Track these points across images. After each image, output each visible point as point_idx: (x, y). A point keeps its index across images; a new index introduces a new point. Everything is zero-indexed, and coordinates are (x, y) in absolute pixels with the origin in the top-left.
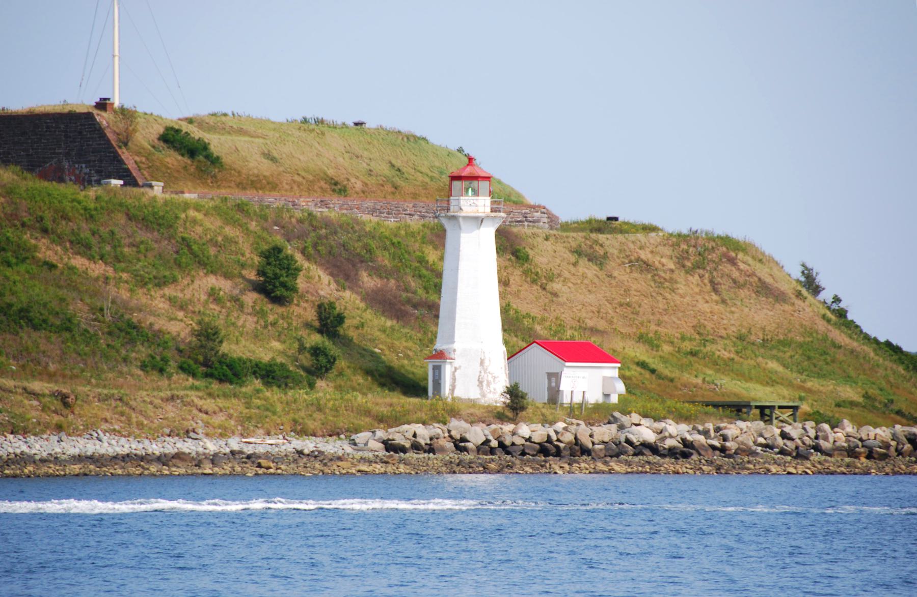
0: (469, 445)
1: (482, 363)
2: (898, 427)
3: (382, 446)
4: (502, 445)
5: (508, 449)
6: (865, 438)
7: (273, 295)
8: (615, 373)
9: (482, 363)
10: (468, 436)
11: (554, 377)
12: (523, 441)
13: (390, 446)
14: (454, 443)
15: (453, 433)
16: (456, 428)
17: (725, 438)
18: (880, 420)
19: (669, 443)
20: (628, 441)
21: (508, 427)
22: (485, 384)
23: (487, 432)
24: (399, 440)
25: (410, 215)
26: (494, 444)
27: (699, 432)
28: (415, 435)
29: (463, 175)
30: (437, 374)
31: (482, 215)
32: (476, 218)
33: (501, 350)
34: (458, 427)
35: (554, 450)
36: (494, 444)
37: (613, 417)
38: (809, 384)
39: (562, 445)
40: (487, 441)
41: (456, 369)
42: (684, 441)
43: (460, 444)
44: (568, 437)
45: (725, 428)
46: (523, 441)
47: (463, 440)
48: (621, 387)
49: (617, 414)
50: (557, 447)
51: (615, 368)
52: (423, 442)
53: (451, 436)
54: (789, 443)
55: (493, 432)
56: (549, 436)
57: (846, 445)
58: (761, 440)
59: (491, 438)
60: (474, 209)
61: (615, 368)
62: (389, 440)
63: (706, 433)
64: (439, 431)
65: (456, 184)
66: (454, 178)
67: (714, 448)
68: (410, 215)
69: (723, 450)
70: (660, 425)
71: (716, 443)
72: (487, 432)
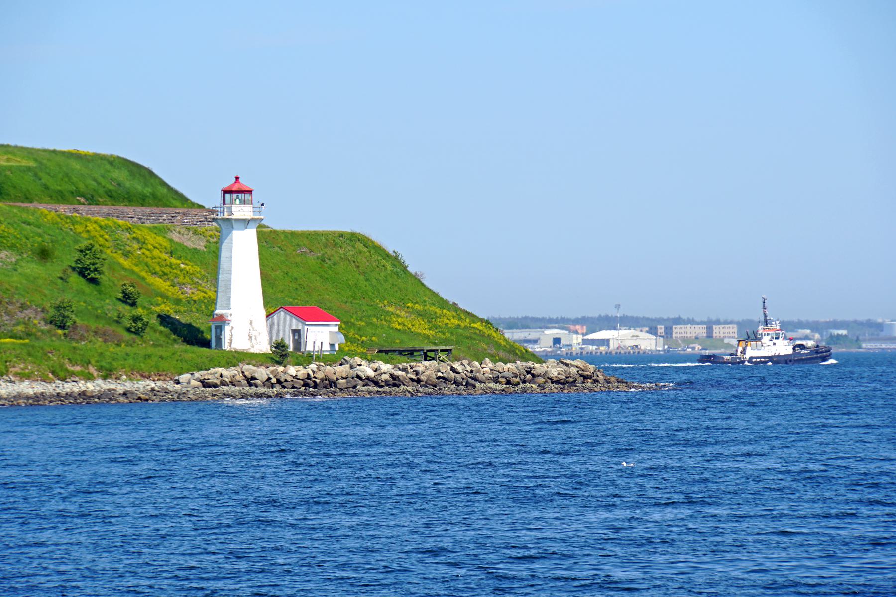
0: (258, 382)
1: (251, 323)
2: (518, 362)
3: (200, 383)
4: (279, 381)
5: (283, 384)
6: (501, 370)
7: (89, 277)
8: (336, 329)
9: (251, 323)
10: (256, 375)
11: (296, 332)
12: (292, 378)
13: (205, 383)
14: (247, 380)
15: (246, 373)
16: (248, 370)
17: (417, 373)
18: (177, 323)
19: (385, 377)
20: (358, 377)
21: (281, 368)
22: (253, 338)
23: (268, 373)
24: (213, 380)
25: (132, 218)
26: (274, 380)
27: (399, 369)
28: (221, 375)
29: (234, 189)
30: (218, 331)
31: (249, 218)
32: (244, 220)
33: (263, 313)
34: (249, 369)
35: (312, 384)
36: (274, 380)
37: (345, 359)
38: (595, 347)
39: (318, 381)
40: (269, 379)
41: (232, 328)
42: (392, 375)
43: (251, 380)
44: (320, 375)
45: (416, 366)
46: (292, 378)
47: (254, 378)
48: (342, 339)
49: (347, 358)
50: (315, 382)
51: (336, 325)
52: (228, 380)
53: (245, 376)
54: (457, 375)
55: (272, 372)
56: (308, 374)
57: (491, 376)
58: (439, 374)
59: (271, 376)
60: (243, 213)
61: (336, 325)
62: (205, 379)
63: (405, 370)
64: (236, 372)
65: (228, 196)
66: (225, 192)
67: (412, 379)
68: (132, 218)
69: (419, 381)
70: (376, 365)
71: (414, 377)
72: (268, 373)
